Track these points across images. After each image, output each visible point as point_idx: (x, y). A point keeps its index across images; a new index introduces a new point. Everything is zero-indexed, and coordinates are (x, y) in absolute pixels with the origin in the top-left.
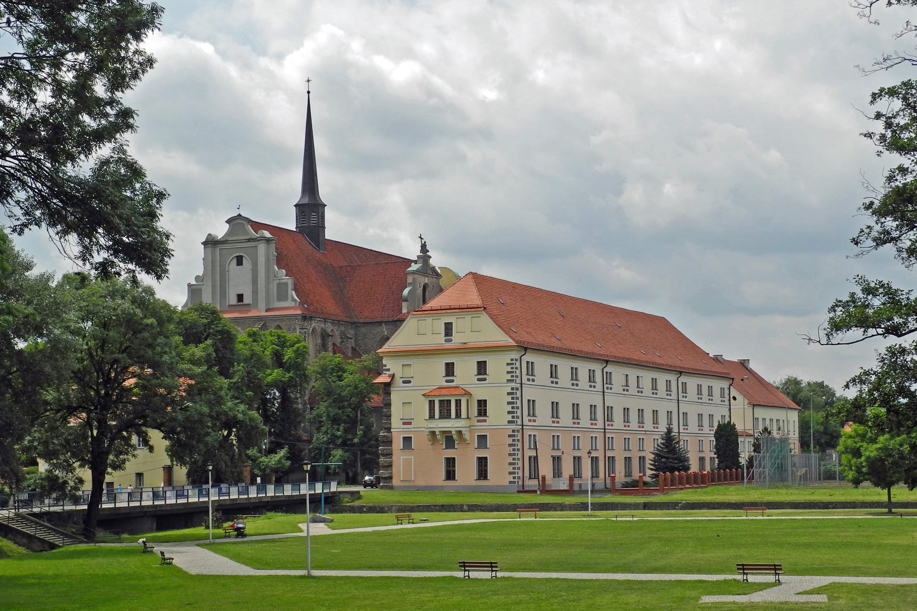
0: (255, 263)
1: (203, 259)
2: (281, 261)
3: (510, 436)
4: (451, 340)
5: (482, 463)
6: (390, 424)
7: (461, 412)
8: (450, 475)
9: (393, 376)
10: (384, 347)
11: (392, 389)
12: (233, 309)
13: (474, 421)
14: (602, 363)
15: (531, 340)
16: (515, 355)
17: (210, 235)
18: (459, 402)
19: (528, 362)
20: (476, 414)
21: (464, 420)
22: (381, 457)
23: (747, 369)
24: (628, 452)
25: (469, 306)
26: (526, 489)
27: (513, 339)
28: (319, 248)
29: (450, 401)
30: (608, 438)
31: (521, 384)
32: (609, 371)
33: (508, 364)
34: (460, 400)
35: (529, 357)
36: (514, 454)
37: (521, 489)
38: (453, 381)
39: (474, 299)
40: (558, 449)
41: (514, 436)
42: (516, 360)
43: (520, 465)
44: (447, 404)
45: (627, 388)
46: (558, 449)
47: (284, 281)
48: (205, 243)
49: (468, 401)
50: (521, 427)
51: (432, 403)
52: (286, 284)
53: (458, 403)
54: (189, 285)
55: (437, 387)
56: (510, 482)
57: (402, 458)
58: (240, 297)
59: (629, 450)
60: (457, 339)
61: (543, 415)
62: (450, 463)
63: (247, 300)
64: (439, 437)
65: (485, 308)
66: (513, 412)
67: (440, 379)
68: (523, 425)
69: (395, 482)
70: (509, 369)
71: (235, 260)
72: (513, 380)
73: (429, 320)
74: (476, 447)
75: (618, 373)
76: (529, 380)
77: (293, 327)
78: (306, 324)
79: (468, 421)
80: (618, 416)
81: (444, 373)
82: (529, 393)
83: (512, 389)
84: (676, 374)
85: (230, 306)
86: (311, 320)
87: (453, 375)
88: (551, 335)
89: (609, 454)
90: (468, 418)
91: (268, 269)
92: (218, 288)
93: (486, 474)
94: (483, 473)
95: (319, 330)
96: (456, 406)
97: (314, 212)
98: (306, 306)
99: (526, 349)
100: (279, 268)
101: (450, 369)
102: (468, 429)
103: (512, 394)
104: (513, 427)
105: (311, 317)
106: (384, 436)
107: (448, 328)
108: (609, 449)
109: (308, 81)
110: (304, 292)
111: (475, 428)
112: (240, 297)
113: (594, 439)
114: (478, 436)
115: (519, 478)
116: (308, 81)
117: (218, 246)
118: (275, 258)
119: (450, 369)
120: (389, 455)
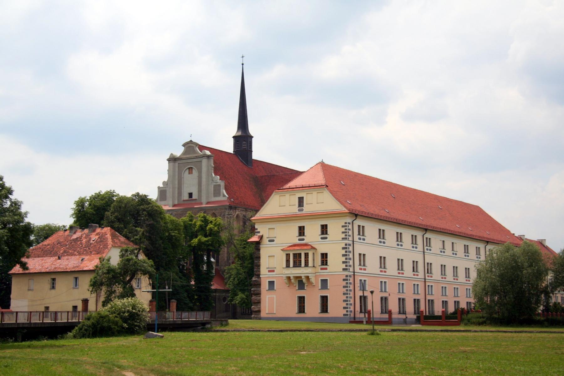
0: (200, 172)
1: (168, 170)
2: (217, 171)
3: (344, 280)
4: (302, 210)
5: (324, 299)
6: (259, 271)
7: (308, 262)
8: (302, 309)
9: (261, 237)
10: (256, 216)
11: (261, 246)
12: (186, 202)
13: (318, 269)
14: (423, 231)
15: (363, 209)
16: (349, 220)
17: (172, 154)
18: (307, 255)
19: (359, 226)
20: (320, 263)
21: (311, 268)
22: (253, 296)
23: (544, 246)
24: (444, 297)
25: (316, 185)
26: (357, 320)
27: (345, 207)
28: (248, 164)
29: (301, 254)
30: (429, 286)
31: (353, 241)
32: (429, 237)
33: (343, 226)
34: (308, 253)
35: (359, 222)
36: (347, 294)
37: (353, 320)
38: (303, 240)
39: (321, 180)
40: (385, 291)
41: (347, 280)
42: (349, 223)
43: (352, 302)
44: (299, 256)
45: (444, 250)
46: (385, 291)
47: (218, 183)
48: (169, 160)
49: (314, 254)
50: (353, 273)
51: (288, 255)
52: (219, 185)
53: (307, 255)
54: (159, 188)
55: (292, 244)
56: (344, 315)
57: (267, 296)
58: (191, 195)
59: (445, 295)
60: (307, 209)
61: (373, 265)
62: (301, 300)
63: (194, 197)
64: (293, 281)
65: (327, 186)
66: (346, 262)
67: (294, 238)
68: (354, 272)
69: (263, 314)
70: (343, 229)
71: (188, 171)
72: (346, 238)
73: (287, 196)
74: (297, 289)
75: (436, 240)
76: (360, 239)
77: (223, 214)
78: (231, 211)
79: (314, 268)
80: (436, 270)
81: (297, 234)
82: (359, 248)
83: (346, 245)
84: (484, 243)
85: (184, 201)
86: (235, 209)
87: (304, 235)
88: (381, 209)
89: (428, 297)
90: (314, 266)
91: (209, 175)
92: (177, 189)
93: (327, 308)
94: (324, 308)
95: (241, 216)
96: (305, 258)
97: (245, 141)
98: (232, 200)
99: (356, 215)
100: (216, 174)
101: (301, 230)
102: (314, 275)
103: (346, 248)
104: (346, 273)
105: (236, 207)
106: (255, 281)
107: (301, 200)
108: (429, 294)
109: (243, 57)
110: (232, 191)
111: (318, 274)
112: (191, 195)
113: (416, 286)
114: (269, 282)
115: (351, 311)
116: (243, 57)
117: (177, 161)
118: (213, 169)
119: (301, 230)
120: (259, 294)
